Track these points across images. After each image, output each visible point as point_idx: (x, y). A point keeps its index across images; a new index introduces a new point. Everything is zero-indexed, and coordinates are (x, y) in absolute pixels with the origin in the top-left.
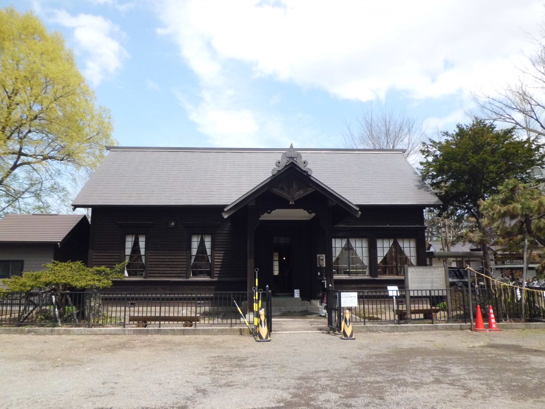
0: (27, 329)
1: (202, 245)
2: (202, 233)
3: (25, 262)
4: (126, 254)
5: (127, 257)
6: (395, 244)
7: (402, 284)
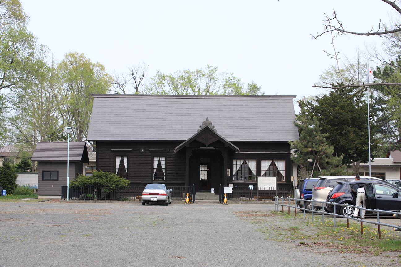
0: (268, 201)
1: (122, 162)
2: (159, 156)
3: (386, 174)
4: (154, 167)
5: (117, 169)
6: (273, 164)
7: (256, 185)
